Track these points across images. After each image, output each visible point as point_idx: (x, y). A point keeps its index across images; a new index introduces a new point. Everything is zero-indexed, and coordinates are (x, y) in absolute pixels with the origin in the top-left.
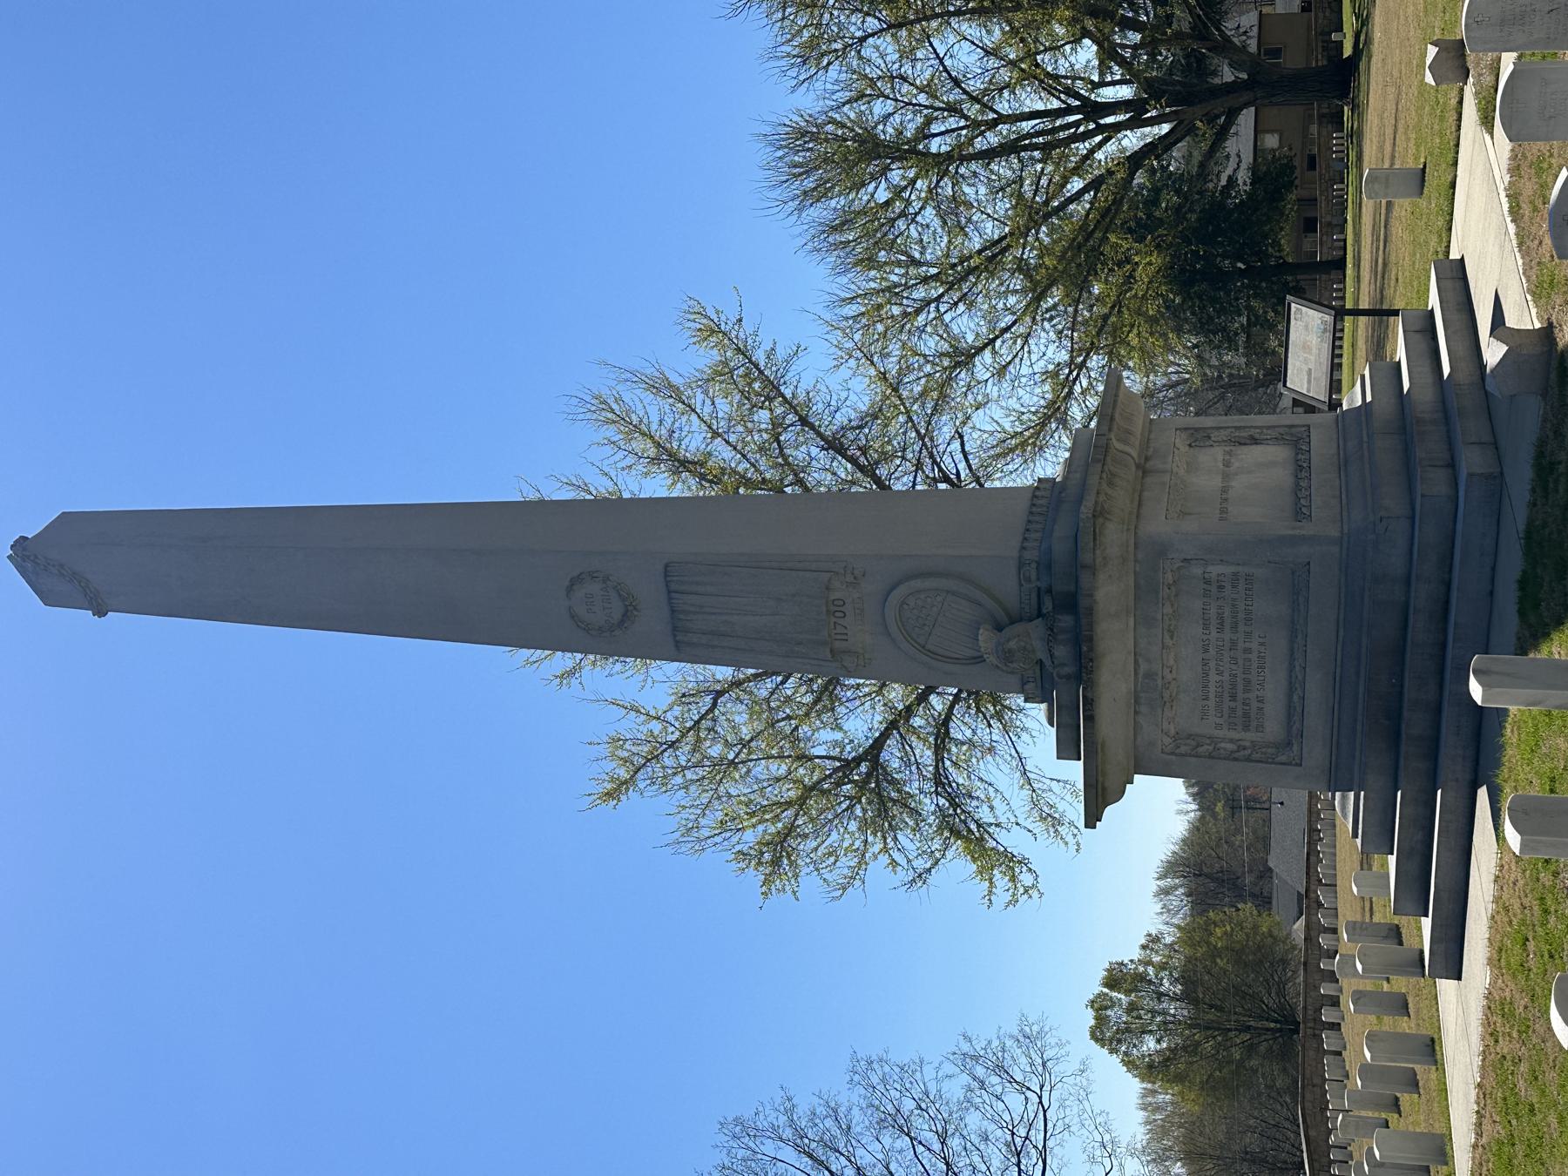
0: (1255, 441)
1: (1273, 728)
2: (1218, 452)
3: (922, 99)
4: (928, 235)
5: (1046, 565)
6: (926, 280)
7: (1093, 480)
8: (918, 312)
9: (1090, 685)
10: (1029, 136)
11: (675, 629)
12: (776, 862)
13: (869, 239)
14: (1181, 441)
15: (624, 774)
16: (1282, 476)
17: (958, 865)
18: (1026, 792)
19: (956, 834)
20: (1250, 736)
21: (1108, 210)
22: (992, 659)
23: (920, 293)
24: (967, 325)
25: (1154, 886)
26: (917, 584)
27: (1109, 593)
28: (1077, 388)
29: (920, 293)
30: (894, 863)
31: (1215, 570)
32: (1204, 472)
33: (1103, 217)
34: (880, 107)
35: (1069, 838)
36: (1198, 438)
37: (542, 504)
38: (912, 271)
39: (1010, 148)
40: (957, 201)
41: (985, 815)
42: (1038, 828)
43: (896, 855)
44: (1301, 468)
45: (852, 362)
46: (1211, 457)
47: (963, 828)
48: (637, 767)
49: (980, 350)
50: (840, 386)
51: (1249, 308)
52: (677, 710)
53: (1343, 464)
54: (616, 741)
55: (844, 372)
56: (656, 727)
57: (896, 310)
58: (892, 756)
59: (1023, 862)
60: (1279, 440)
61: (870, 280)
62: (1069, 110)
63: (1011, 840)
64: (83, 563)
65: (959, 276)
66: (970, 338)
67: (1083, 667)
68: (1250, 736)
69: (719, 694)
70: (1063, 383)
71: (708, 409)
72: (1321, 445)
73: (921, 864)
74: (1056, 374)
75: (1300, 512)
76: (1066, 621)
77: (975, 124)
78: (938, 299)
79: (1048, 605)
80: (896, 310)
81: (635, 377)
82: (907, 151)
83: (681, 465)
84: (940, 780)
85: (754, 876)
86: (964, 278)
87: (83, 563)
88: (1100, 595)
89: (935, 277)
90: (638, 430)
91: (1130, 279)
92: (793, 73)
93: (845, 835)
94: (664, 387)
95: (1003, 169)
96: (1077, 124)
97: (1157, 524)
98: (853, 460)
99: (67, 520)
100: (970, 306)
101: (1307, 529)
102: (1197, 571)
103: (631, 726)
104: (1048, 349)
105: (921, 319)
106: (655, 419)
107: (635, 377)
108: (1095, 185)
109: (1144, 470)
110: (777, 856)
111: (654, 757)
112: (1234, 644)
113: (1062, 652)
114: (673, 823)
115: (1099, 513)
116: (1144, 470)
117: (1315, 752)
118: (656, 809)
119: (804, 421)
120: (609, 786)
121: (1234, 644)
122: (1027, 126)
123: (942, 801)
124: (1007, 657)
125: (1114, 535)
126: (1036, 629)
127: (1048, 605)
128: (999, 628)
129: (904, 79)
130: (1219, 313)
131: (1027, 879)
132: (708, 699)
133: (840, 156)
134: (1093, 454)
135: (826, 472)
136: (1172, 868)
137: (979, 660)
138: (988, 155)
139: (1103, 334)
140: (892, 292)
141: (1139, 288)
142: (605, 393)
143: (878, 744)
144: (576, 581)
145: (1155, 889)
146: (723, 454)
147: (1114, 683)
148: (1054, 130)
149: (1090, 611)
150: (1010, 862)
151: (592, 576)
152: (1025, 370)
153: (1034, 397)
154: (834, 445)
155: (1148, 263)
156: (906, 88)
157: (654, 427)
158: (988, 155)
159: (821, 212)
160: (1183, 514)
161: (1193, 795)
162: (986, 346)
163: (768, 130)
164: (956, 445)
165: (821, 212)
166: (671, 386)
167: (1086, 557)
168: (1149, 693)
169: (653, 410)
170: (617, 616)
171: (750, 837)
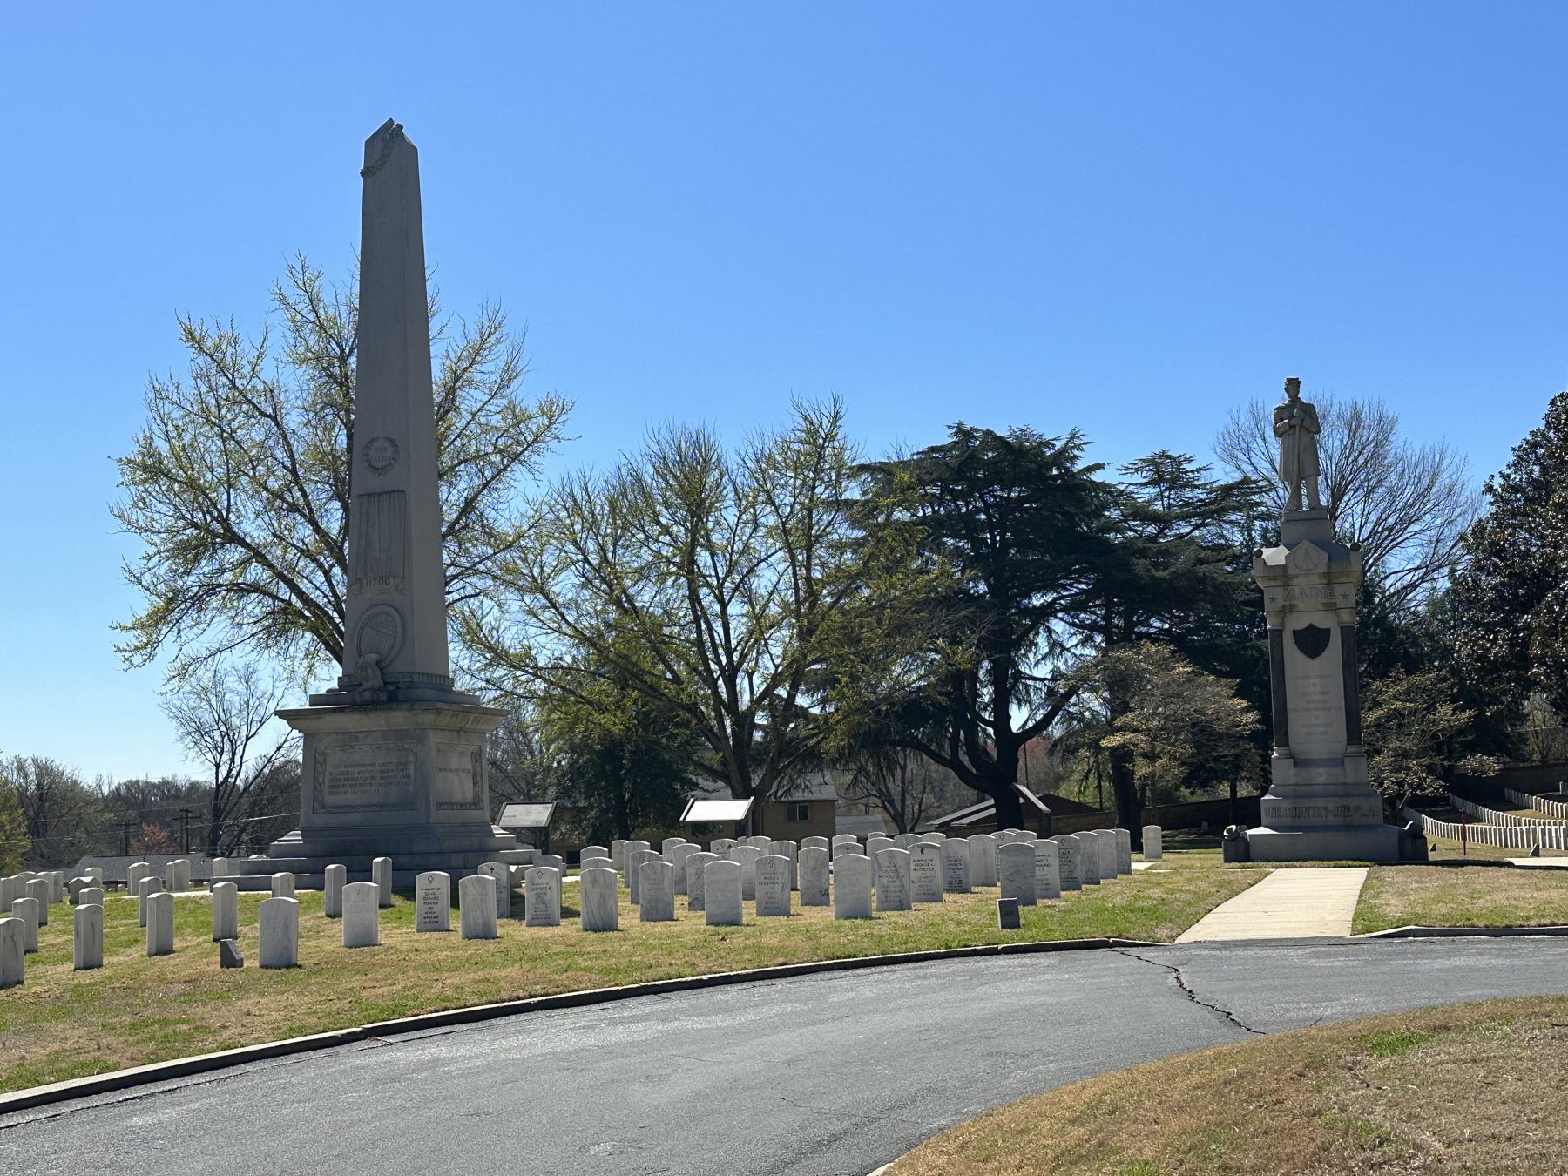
0: (475, 784)
1: (331, 800)
2: (469, 767)
3: (739, 546)
4: (632, 558)
5: (411, 686)
6: (602, 549)
7: (455, 707)
8: (575, 543)
9: (352, 710)
10: (710, 629)
11: (369, 495)
12: (144, 468)
13: (629, 507)
14: (474, 748)
15: (209, 344)
16: (458, 798)
17: (144, 605)
18: (204, 653)
19: (171, 601)
20: (326, 790)
21: (656, 690)
22: (361, 661)
23: (591, 546)
24: (565, 585)
25: (26, 755)
26: (398, 621)
27: (400, 718)
28: (519, 673)
29: (591, 546)
30: (149, 557)
31: (412, 767)
32: (459, 760)
33: (650, 687)
34: (731, 515)
35: (169, 687)
36: (477, 756)
37: (421, 314)
38: (609, 539)
39: (699, 614)
40: (662, 577)
41: (187, 621)
42: (178, 664)
43: (155, 559)
44: (462, 806)
45: (531, 513)
46: (467, 764)
47: (172, 608)
48: (217, 360)
49: (547, 597)
50: (517, 501)
51: (591, 807)
52: (261, 387)
53: (464, 825)
54: (235, 342)
55: (524, 507)
56: (247, 370)
57: (578, 527)
58: (235, 553)
59: (151, 657)
60: (476, 796)
61: (601, 506)
62: (729, 654)
63: (168, 648)
64: (390, 162)
65: (605, 577)
66: (556, 589)
67: (360, 706)
68: (326, 790)
69: (274, 419)
70: (522, 661)
71: (493, 409)
72: (474, 815)
73: (147, 579)
74: (528, 656)
75: (440, 805)
76: (383, 697)
77: (721, 586)
78: (586, 560)
79: (391, 688)
80: (578, 527)
81: (515, 353)
82: (697, 536)
83: (451, 391)
84: (211, 589)
85: (133, 452)
86: (603, 580)
87: (390, 162)
88: (399, 714)
89: (605, 558)
90: (476, 354)
91: (603, 710)
92: (750, 450)
93: (163, 514)
94: (509, 376)
95: (683, 612)
96: (718, 662)
97: (433, 739)
98: (457, 520)
99: (414, 151)
100: (583, 586)
101: (433, 807)
102: (411, 758)
103: (246, 352)
104: (551, 648)
105: (572, 548)
106: (483, 368)
107: (515, 353)
108: (677, 679)
109: (459, 731)
110: (151, 469)
111: (222, 368)
112: (374, 778)
113: (367, 695)
114: (164, 379)
115: (438, 711)
116: (459, 731)
117: (320, 820)
118: (182, 370)
119: (485, 485)
120: (197, 334)
121: (374, 778)
122: (718, 627)
123: (195, 590)
124: (363, 668)
125: (429, 718)
126: (378, 682)
127: (391, 688)
128: (378, 663)
129: (755, 529)
130: (587, 783)
131: (137, 659)
132: (270, 411)
133: (691, 482)
134: (467, 706)
135: (451, 497)
136: (44, 771)
137: (360, 654)
138: (694, 599)
139: (564, 687)
140: (593, 525)
141: (596, 717)
142: (504, 330)
143: (241, 542)
144: (394, 444)
145: (23, 756)
146: (459, 421)
147: (351, 722)
148: (715, 648)
149: (390, 709)
150: (151, 645)
151: (396, 452)
152: (532, 631)
153: (510, 639)
154: (469, 506)
155: (614, 723)
156: (748, 531)
157: (479, 367)
158: (694, 599)
159: (648, 473)
160: (438, 751)
161: (118, 790)
162: (550, 601)
163: (709, 430)
164: (470, 591)
165: (648, 473)
166: (510, 380)
167: (417, 706)
168: (347, 739)
169: (490, 368)
170: (375, 464)
171: (162, 446)
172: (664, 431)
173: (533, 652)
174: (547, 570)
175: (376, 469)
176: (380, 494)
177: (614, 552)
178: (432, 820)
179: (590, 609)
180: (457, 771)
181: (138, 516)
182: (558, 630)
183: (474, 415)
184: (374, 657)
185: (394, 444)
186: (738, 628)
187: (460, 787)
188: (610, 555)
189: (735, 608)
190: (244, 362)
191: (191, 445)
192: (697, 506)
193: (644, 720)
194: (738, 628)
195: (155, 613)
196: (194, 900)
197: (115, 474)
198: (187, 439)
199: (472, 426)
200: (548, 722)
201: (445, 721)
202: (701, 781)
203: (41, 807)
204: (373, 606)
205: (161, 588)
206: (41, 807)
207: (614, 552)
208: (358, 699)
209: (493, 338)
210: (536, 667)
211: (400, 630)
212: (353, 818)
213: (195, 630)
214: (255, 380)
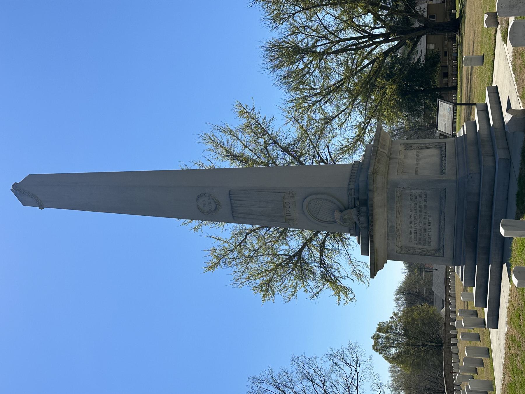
0: (427, 148)
1: (434, 244)
2: (415, 152)
4: (316, 79)
5: (357, 190)
6: (316, 94)
7: (373, 161)
8: (313, 105)
9: (372, 230)
10: (350, 46)
12: (267, 290)
13: (296, 81)
14: (402, 148)
15: (216, 261)
16: (436, 160)
17: (328, 291)
18: (351, 266)
19: (327, 280)
20: (426, 247)
22: (339, 222)
23: (314, 99)
24: (330, 110)
25: (394, 297)
26: (314, 197)
27: (378, 199)
28: (367, 130)
29: (314, 99)
30: (306, 290)
32: (410, 158)
35: (366, 281)
36: (408, 147)
37: (188, 170)
38: (311, 91)
41: (337, 274)
43: (307, 288)
44: (443, 157)
46: (412, 153)
47: (329, 278)
48: (220, 259)
49: (334, 118)
51: (425, 103)
52: (233, 239)
53: (457, 155)
55: (289, 126)
56: (226, 245)
57: (306, 105)
58: (305, 254)
59: (350, 290)
60: (435, 147)
61: (297, 95)
62: (364, 37)
64: (35, 191)
65: (327, 93)
66: (331, 114)
67: (370, 224)
68: (426, 247)
69: (248, 234)
70: (362, 128)
72: (449, 149)
73: (316, 291)
75: (442, 172)
76: (364, 209)
79: (358, 203)
80: (306, 105)
82: (309, 51)
83: (234, 157)
84: (322, 262)
86: (329, 94)
87: (35, 191)
89: (319, 94)
93: (290, 281)
94: (228, 131)
95: (342, 57)
96: (366, 42)
97: (394, 176)
101: (444, 177)
102: (408, 191)
103: (218, 245)
104: (357, 117)
105: (314, 107)
106: (225, 142)
109: (390, 158)
110: (267, 288)
112: (420, 216)
113: (362, 219)
114: (232, 277)
115: (375, 172)
117: (448, 252)
118: (226, 273)
119: (275, 142)
120: (211, 265)
121: (420, 216)
122: (349, 42)
123: (322, 269)
124: (344, 221)
125: (379, 179)
126: (354, 211)
127: (358, 203)
128: (341, 211)
129: (308, 27)
131: (351, 296)
132: (244, 236)
133: (287, 53)
134: (372, 152)
135: (283, 159)
136: (400, 291)
137: (335, 222)
138: (337, 52)
139: (375, 112)
143: (301, 250)
145: (394, 298)
146: (248, 153)
147: (380, 229)
148: (359, 44)
149: (372, 206)
150: (346, 290)
151: (205, 194)
152: (349, 124)
153: (352, 134)
154: (285, 150)
155: (391, 88)
156: (309, 30)
157: (225, 144)
158: (337, 52)
160: (403, 172)
162: (336, 116)
163: (263, 45)
164: (326, 150)
167: (370, 187)
168: (392, 232)
169: (224, 138)
171: (258, 282)
172: (266, 66)
173: (358, 123)
174: (322, 117)
175: (216, 208)
176: (232, 206)
177: (316, 89)
178: (454, 178)
179: (342, 99)
180: (417, 160)
181: (291, 290)
182: (350, 113)
183: (246, 147)
184: (337, 215)
185: (199, 196)
186: (351, 34)
187: (429, 158)
188: (318, 91)
189: (342, 36)
190: (222, 246)
191: (257, 271)
192: (297, 51)
193: (388, 77)
194: (351, 34)
195: (332, 287)
196: (510, 358)
197: (268, 303)
198: (255, 273)
199: (251, 148)
200: (389, 118)
201: (382, 168)
202: (418, 57)
203: (412, 294)
204: (304, 214)
205: (321, 284)
206: (412, 294)
207: (316, 89)
208: (365, 225)
209: (212, 138)
210: (365, 122)
211: (319, 196)
212: (448, 231)
213: (341, 270)
214: (231, 241)
